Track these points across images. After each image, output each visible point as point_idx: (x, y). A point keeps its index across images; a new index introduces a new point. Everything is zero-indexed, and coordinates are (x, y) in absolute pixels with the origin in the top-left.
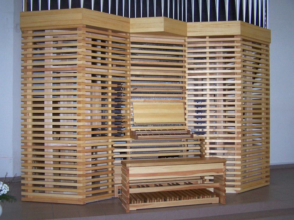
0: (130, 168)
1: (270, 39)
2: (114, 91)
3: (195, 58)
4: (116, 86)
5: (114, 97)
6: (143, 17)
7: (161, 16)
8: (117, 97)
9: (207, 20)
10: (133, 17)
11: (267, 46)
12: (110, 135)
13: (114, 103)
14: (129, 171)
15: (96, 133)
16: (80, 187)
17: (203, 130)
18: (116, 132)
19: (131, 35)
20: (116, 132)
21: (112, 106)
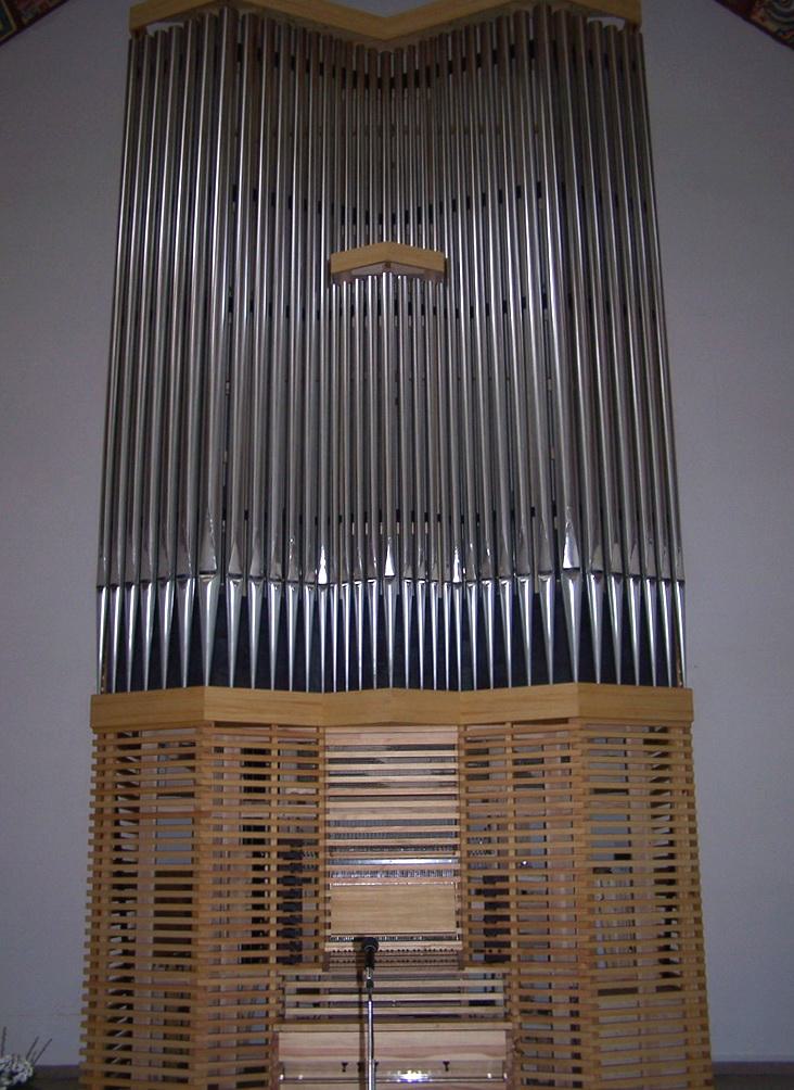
0: (281, 1035)
1: (692, 712)
2: (281, 861)
3: (434, 772)
4: (286, 848)
5: (282, 874)
6: (513, 686)
7: (571, 680)
8: (288, 873)
9: (650, 683)
10: (383, 687)
11: (686, 731)
12: (273, 960)
13: (281, 887)
14: (280, 1042)
15: (252, 955)
16: (565, 1072)
17: (499, 951)
18: (287, 953)
19: (328, 730)
20: (287, 953)
21: (279, 894)
